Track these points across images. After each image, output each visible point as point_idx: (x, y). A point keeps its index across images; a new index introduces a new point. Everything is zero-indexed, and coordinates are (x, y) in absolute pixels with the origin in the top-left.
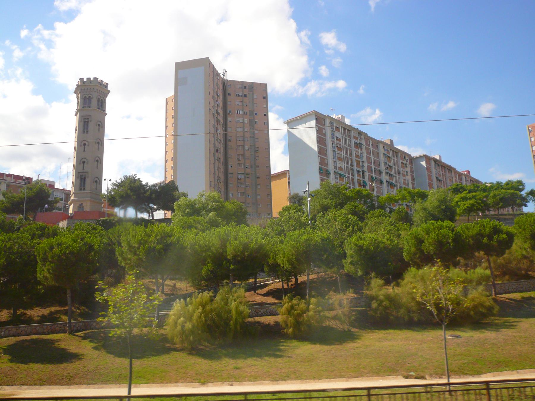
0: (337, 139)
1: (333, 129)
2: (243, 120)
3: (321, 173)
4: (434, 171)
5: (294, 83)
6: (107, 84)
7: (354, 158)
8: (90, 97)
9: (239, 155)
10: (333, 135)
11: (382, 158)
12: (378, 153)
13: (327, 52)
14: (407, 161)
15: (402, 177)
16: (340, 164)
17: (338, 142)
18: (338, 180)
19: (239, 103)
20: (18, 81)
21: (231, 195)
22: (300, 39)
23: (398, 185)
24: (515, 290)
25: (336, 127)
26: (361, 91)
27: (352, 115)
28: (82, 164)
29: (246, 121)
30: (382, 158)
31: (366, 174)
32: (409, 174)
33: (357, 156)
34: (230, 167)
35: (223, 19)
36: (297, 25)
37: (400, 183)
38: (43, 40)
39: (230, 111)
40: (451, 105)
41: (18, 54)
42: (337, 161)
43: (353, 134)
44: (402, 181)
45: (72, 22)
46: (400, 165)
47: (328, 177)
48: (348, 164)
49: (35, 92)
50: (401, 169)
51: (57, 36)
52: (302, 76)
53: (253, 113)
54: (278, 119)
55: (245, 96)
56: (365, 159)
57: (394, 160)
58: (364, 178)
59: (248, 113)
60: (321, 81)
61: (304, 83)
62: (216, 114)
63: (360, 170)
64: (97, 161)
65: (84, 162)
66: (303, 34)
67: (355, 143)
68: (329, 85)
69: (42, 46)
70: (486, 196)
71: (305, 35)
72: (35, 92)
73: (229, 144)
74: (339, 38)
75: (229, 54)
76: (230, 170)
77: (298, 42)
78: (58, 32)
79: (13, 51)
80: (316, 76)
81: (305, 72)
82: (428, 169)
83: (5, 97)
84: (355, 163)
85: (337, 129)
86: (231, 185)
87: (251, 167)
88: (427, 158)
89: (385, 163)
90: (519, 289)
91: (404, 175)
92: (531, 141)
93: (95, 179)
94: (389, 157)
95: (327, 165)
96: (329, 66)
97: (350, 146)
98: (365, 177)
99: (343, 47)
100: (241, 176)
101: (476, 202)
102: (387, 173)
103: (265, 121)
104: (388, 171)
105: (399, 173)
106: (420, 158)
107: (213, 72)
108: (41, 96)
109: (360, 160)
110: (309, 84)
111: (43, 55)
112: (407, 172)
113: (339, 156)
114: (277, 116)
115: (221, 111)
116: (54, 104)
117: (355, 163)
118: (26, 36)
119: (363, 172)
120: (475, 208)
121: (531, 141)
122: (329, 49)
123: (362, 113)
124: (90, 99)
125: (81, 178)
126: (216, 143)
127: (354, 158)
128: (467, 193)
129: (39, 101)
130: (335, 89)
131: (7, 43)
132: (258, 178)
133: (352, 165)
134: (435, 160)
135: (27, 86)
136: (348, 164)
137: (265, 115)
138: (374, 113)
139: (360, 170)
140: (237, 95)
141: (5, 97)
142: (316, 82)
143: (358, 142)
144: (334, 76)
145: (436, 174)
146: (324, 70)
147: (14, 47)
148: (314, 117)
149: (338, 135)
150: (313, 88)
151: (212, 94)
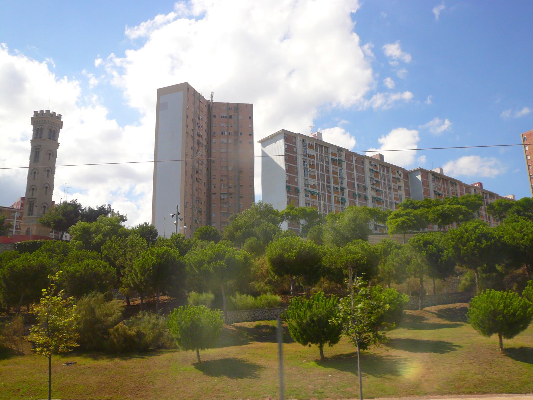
0: (309, 157)
1: (306, 146)
2: (228, 140)
3: (288, 192)
5: (359, 96)
6: (60, 115)
7: (331, 175)
8: (42, 128)
9: (222, 176)
10: (305, 154)
11: (367, 174)
12: (363, 169)
13: (391, 63)
14: (400, 175)
15: (393, 192)
16: (311, 182)
17: (311, 159)
18: (310, 199)
19: (224, 124)
20: (94, 107)
21: (214, 215)
22: (364, 52)
23: (388, 200)
24: (267, 317)
25: (309, 144)
26: (429, 102)
27: (420, 127)
28: (32, 191)
29: (230, 141)
30: (367, 174)
31: (346, 191)
32: (403, 188)
33: (335, 173)
34: (213, 187)
35: (286, 37)
36: (360, 38)
37: (390, 198)
38: (115, 67)
39: (214, 133)
40: (526, 111)
41: (93, 81)
42: (309, 178)
43: (330, 151)
44: (393, 196)
45: (141, 49)
46: (391, 179)
47: (298, 196)
48: (324, 181)
49: (110, 117)
50: (392, 184)
51: (128, 62)
52: (367, 89)
54: (344, 133)
55: (231, 117)
56: (345, 175)
57: (384, 175)
58: (343, 194)
59: (232, 134)
60: (386, 94)
61: (369, 96)
62: (197, 138)
63: (339, 186)
64: (47, 188)
65: (33, 189)
66: (366, 47)
67: (333, 160)
68: (395, 97)
69: (115, 73)
70: (427, 212)
71: (369, 48)
72: (110, 117)
73: (213, 165)
74: (404, 49)
75: (293, 71)
76: (213, 190)
77: (362, 55)
78: (128, 59)
79: (89, 79)
80: (382, 89)
81: (370, 85)
82: (425, 183)
83: (82, 122)
84: (332, 180)
85: (311, 146)
86: (213, 205)
87: (235, 186)
88: (424, 173)
89: (372, 179)
90: (272, 317)
91: (396, 190)
92: (525, 150)
93: (44, 205)
94: (377, 172)
95: (297, 183)
96: (395, 78)
97: (327, 163)
98: (345, 194)
99: (408, 58)
100: (224, 196)
101: (408, 219)
102: (373, 189)
103: (250, 141)
104: (375, 187)
105: (390, 188)
106: (416, 172)
107: (194, 95)
108: (115, 120)
109: (339, 177)
110: (374, 97)
111: (116, 82)
112: (400, 187)
114: (343, 131)
115: (204, 134)
116: (127, 127)
117: (332, 180)
119: (342, 189)
120: (406, 225)
121: (525, 150)
122: (393, 60)
123: (431, 123)
125: (30, 204)
126: (196, 165)
127: (331, 175)
128: (402, 210)
129: (113, 125)
130: (401, 101)
131: (84, 72)
132: (242, 197)
133: (328, 182)
134: (434, 174)
135: (102, 111)
136: (324, 181)
137: (250, 135)
138: (443, 123)
139: (339, 186)
140: (223, 117)
141: (82, 122)
142: (382, 94)
143: (337, 158)
144: (400, 87)
145: (434, 188)
146: (389, 83)
147: (90, 75)
148: (283, 135)
150: (378, 101)
151: (191, 116)
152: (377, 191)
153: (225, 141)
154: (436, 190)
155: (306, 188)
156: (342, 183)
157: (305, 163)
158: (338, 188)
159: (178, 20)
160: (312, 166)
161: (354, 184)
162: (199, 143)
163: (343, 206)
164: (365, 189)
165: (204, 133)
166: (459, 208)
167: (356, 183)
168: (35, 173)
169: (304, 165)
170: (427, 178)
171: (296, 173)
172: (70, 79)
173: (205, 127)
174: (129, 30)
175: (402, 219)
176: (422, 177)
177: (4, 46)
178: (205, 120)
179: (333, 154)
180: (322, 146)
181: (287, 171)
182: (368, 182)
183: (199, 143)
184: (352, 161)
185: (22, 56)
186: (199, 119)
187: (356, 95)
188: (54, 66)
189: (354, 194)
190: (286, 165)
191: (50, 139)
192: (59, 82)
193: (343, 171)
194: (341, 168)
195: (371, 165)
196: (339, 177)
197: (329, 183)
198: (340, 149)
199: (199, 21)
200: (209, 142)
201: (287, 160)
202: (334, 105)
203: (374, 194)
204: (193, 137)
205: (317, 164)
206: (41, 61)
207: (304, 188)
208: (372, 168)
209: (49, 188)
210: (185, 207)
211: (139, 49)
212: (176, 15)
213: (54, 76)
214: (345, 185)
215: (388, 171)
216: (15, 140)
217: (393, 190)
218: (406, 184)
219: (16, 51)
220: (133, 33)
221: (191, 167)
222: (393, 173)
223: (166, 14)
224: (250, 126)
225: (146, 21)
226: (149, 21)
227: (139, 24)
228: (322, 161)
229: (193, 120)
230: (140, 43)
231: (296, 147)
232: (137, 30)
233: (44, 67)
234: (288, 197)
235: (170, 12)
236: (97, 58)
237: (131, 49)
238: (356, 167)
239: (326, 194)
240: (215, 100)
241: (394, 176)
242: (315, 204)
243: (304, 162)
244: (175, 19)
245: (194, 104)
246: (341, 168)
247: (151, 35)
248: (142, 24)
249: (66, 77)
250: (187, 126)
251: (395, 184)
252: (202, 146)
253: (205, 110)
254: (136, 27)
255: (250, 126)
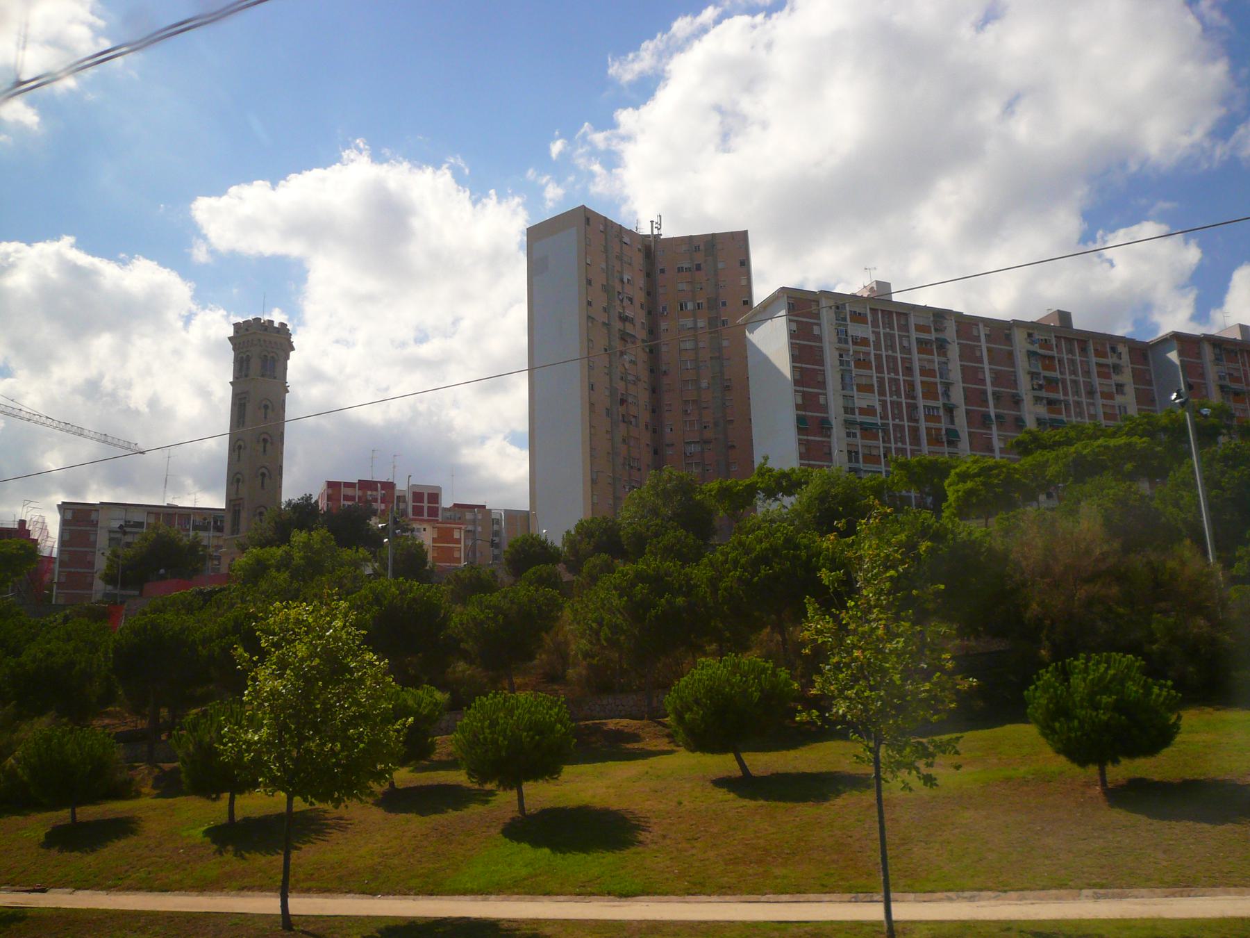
0: (855, 343)
1: (844, 319)
3: (801, 430)
4: (1212, 373)
5: (1198, 134)
9: (686, 402)
10: (842, 336)
12: (1010, 355)
15: (1100, 401)
16: (861, 401)
17: (858, 348)
18: (859, 441)
19: (684, 286)
22: (1200, 18)
29: (701, 324)
32: (1130, 389)
33: (924, 372)
38: (594, 153)
39: (664, 309)
42: (855, 393)
43: (912, 321)
44: (1100, 411)
46: (1094, 370)
48: (898, 394)
50: (1096, 381)
52: (1218, 112)
53: (715, 303)
55: (698, 268)
62: (618, 325)
63: (940, 403)
65: (238, 481)
67: (919, 341)
69: (596, 168)
78: (622, 131)
79: (542, 188)
81: (1226, 100)
82: (1192, 369)
85: (858, 318)
89: (1033, 375)
94: (1052, 358)
95: (825, 408)
98: (956, 420)
100: (692, 449)
101: (984, 484)
102: (1038, 399)
104: (1044, 394)
105: (1091, 393)
113: (863, 381)
118: (561, 154)
119: (950, 410)
124: (248, 359)
126: (621, 385)
127: (918, 378)
131: (531, 173)
133: (911, 395)
137: (745, 303)
140: (680, 270)
145: (1220, 378)
148: (784, 301)
149: (856, 330)
152: (1051, 402)
153: (690, 325)
154: (1227, 382)
155: (850, 416)
156: (948, 396)
157: (845, 358)
158: (938, 408)
159: (726, 22)
160: (863, 363)
161: (984, 392)
162: (624, 337)
163: (952, 450)
164: (1017, 401)
165: (636, 314)
166: (1130, 445)
167: (989, 389)
168: (240, 447)
169: (842, 363)
170: (1199, 355)
171: (822, 385)
172: (501, 197)
173: (640, 297)
174: (617, 65)
175: (969, 484)
176: (1180, 354)
177: (361, 145)
178: (640, 281)
179: (919, 328)
180: (890, 313)
181: (797, 382)
182: (1024, 385)
183: (624, 337)
184: (978, 339)
185: (398, 162)
186: (622, 281)
187: (1188, 132)
188: (467, 171)
189: (986, 416)
190: (794, 369)
191: (263, 376)
192: (479, 206)
193: (950, 366)
194: (943, 359)
195: (1032, 343)
196: (938, 380)
197: (914, 398)
198: (940, 315)
199: (775, 16)
200: (653, 331)
201: (795, 358)
202: (1133, 167)
203: (1042, 411)
204: (607, 325)
205: (878, 357)
206: (437, 166)
207: (842, 416)
208: (1036, 348)
209: (271, 473)
210: (594, 482)
211: (645, 103)
212: (719, 10)
213: (468, 193)
214: (957, 396)
215: (1084, 350)
216: (403, 345)
217: (1098, 395)
218: (1138, 377)
219: (386, 152)
220: (627, 70)
221: (607, 393)
222: (1098, 353)
223: (697, 12)
224: (744, 282)
225: (652, 37)
226: (659, 36)
227: (636, 47)
228: (893, 347)
229: (606, 289)
230: (645, 89)
231: (819, 325)
232: (633, 60)
233: (444, 178)
234: (800, 442)
235: (706, 7)
236: (554, 139)
237: (625, 108)
238: (989, 350)
239: (906, 424)
240: (667, 232)
241: (1102, 360)
242: (874, 452)
243: (841, 356)
244: (718, 21)
245: (606, 251)
246: (943, 359)
247: (667, 68)
248: (644, 45)
249: (492, 192)
250: (590, 304)
251: (1103, 381)
252: (634, 343)
253: (639, 260)
254: (631, 56)
255: (744, 282)
